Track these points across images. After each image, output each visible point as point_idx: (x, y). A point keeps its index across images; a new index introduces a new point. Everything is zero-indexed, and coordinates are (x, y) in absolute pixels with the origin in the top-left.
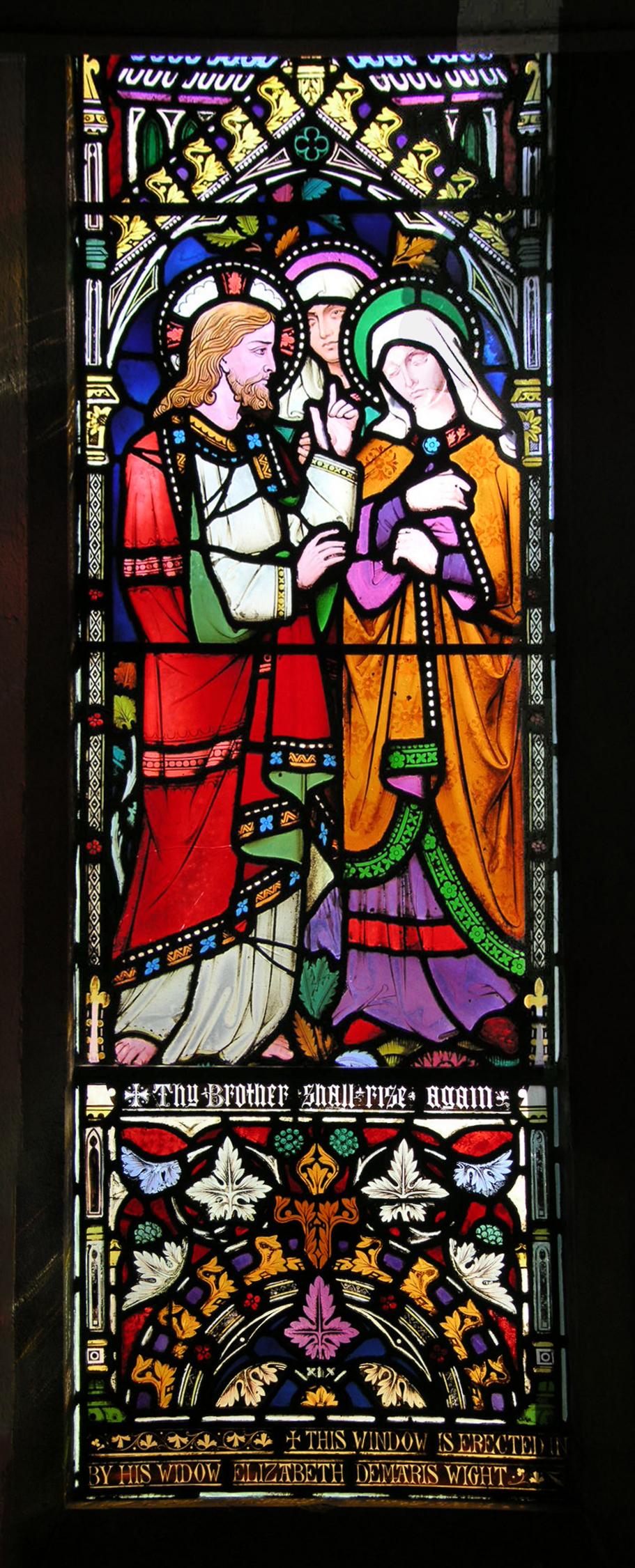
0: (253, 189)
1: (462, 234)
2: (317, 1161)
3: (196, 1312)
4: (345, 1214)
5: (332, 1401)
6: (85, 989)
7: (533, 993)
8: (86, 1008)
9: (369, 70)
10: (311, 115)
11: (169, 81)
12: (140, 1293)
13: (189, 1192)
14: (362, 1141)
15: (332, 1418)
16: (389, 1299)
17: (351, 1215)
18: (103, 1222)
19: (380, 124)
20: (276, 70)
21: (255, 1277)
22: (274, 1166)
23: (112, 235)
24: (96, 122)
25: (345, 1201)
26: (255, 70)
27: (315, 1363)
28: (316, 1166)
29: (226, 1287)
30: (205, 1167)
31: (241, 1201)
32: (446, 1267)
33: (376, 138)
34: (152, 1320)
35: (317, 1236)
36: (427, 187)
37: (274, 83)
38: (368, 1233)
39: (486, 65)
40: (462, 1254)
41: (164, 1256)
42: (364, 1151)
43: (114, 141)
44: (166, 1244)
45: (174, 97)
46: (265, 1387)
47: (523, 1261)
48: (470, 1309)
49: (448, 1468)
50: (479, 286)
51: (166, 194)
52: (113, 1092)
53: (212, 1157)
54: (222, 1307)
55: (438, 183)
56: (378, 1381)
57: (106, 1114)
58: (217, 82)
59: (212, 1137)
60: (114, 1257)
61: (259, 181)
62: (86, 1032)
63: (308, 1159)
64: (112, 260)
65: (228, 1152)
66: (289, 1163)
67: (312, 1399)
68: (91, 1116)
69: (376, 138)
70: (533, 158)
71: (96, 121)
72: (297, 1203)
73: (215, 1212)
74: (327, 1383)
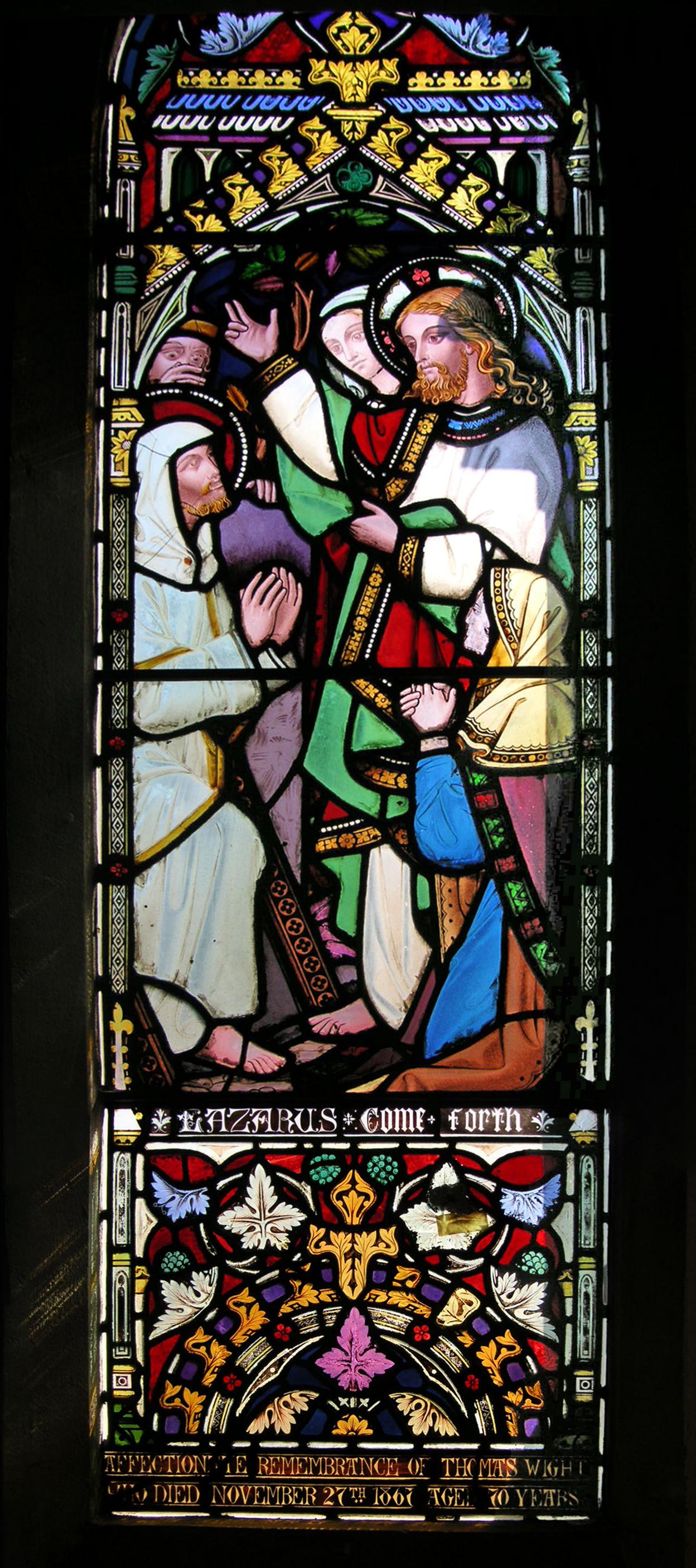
0: (295, 215)
1: (513, 264)
2: (353, 1188)
3: (224, 1340)
4: (382, 1245)
5: (363, 1427)
6: (108, 1017)
7: (584, 1015)
8: (110, 1035)
9: (415, 114)
10: (354, 153)
11: (206, 124)
12: (165, 1324)
13: (221, 1220)
14: (402, 1167)
15: (363, 1445)
16: (426, 1330)
17: (388, 1246)
18: (130, 1248)
19: (427, 160)
20: (316, 111)
21: (285, 1309)
22: (307, 1191)
23: (144, 263)
24: (130, 161)
25: (383, 1232)
26: (295, 112)
27: (347, 1394)
28: (353, 1193)
29: (257, 1318)
30: (238, 1195)
31: (275, 1230)
32: (488, 1298)
33: (423, 174)
34: (180, 1348)
35: (353, 1267)
36: (478, 219)
37: (316, 123)
38: (407, 1264)
39: (535, 113)
40: (504, 1283)
41: (192, 1285)
42: (403, 1177)
43: (147, 176)
44: (194, 1274)
45: (213, 137)
46: (296, 1415)
47: (568, 1288)
48: (507, 1339)
49: (527, 1461)
50: (532, 312)
51: (203, 223)
52: (140, 1116)
53: (244, 1183)
54: (251, 1340)
55: (488, 217)
56: (411, 1411)
57: (132, 1139)
58: (256, 124)
59: (243, 1164)
60: (140, 1285)
61: (301, 208)
62: (110, 1057)
63: (344, 1186)
64: (141, 285)
65: (260, 1180)
66: (322, 1192)
67: (342, 1428)
68: (118, 1141)
69: (423, 174)
70: (583, 197)
71: (130, 160)
72: (332, 1234)
73: (248, 1242)
74: (361, 1412)
